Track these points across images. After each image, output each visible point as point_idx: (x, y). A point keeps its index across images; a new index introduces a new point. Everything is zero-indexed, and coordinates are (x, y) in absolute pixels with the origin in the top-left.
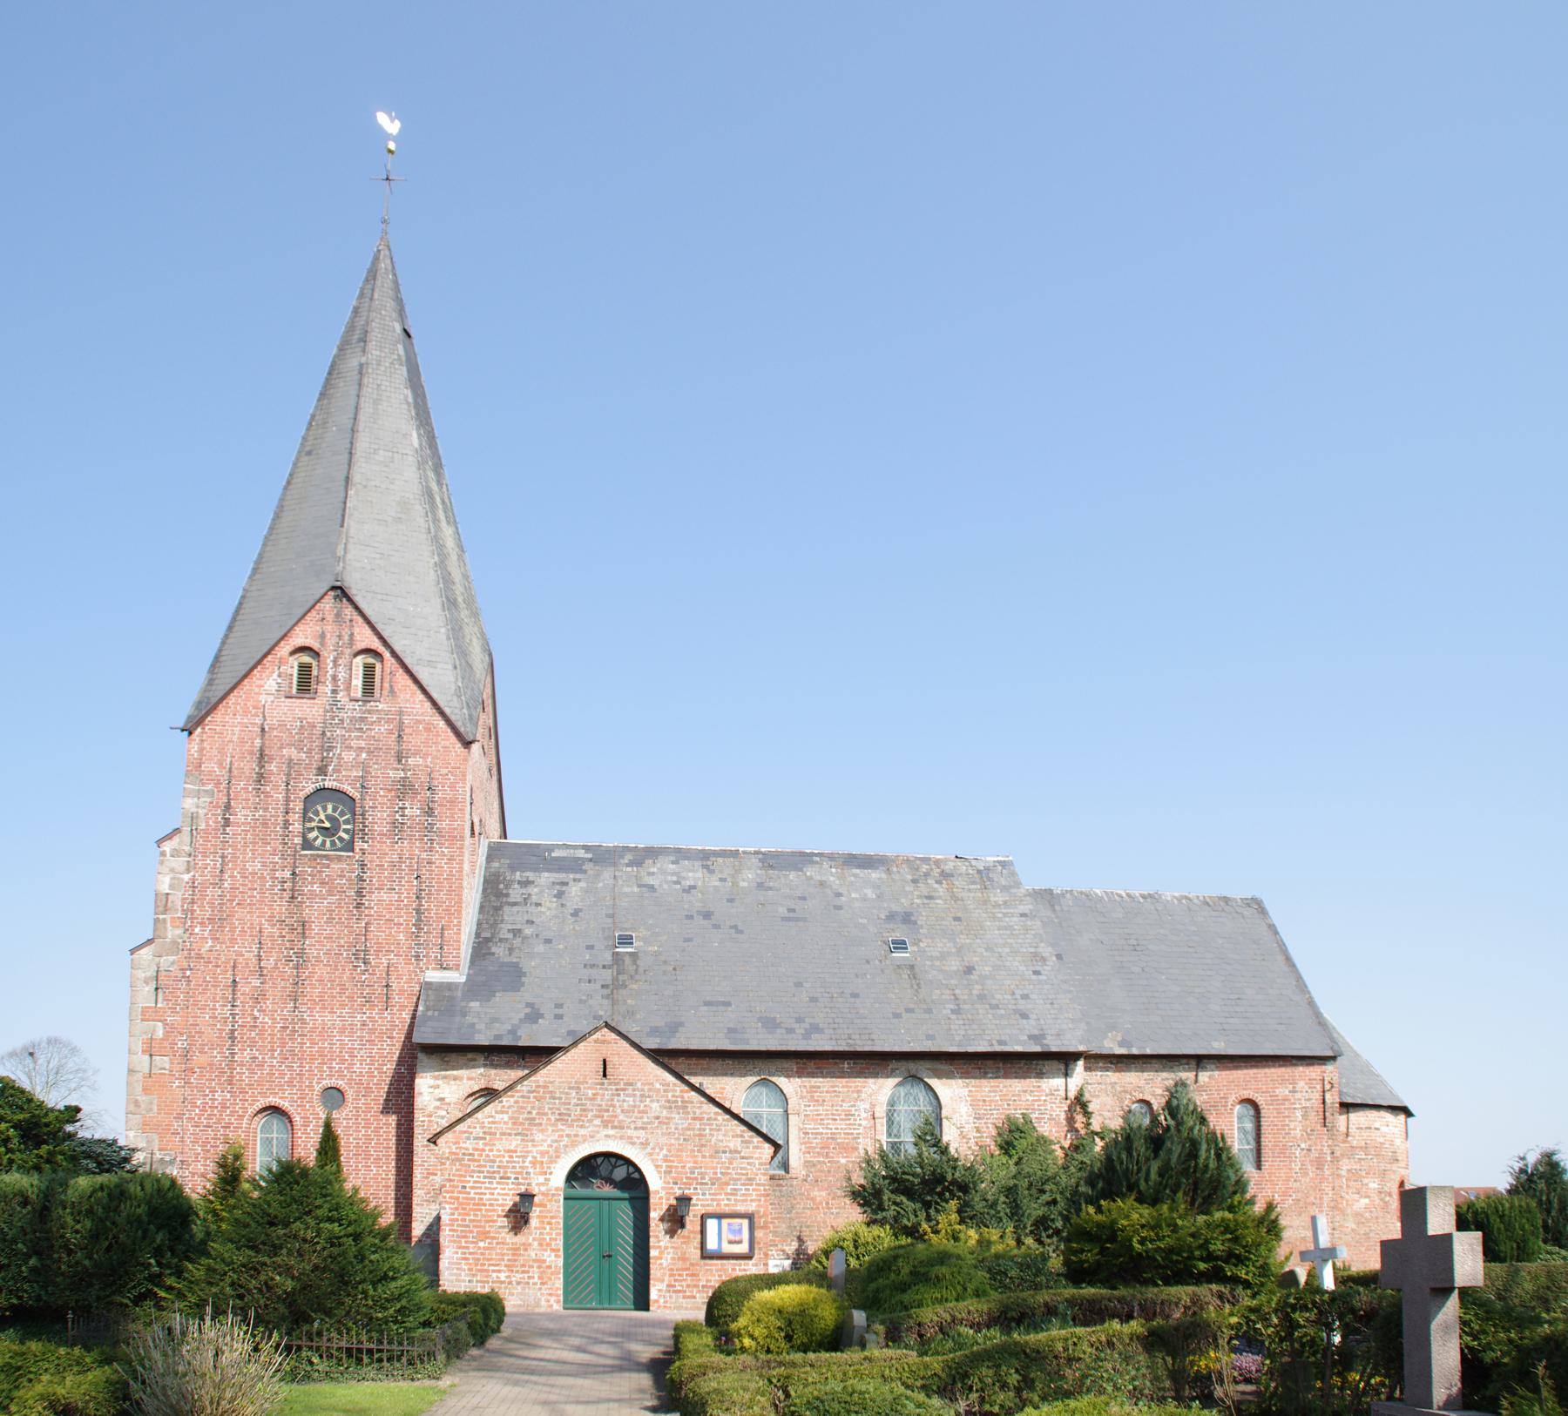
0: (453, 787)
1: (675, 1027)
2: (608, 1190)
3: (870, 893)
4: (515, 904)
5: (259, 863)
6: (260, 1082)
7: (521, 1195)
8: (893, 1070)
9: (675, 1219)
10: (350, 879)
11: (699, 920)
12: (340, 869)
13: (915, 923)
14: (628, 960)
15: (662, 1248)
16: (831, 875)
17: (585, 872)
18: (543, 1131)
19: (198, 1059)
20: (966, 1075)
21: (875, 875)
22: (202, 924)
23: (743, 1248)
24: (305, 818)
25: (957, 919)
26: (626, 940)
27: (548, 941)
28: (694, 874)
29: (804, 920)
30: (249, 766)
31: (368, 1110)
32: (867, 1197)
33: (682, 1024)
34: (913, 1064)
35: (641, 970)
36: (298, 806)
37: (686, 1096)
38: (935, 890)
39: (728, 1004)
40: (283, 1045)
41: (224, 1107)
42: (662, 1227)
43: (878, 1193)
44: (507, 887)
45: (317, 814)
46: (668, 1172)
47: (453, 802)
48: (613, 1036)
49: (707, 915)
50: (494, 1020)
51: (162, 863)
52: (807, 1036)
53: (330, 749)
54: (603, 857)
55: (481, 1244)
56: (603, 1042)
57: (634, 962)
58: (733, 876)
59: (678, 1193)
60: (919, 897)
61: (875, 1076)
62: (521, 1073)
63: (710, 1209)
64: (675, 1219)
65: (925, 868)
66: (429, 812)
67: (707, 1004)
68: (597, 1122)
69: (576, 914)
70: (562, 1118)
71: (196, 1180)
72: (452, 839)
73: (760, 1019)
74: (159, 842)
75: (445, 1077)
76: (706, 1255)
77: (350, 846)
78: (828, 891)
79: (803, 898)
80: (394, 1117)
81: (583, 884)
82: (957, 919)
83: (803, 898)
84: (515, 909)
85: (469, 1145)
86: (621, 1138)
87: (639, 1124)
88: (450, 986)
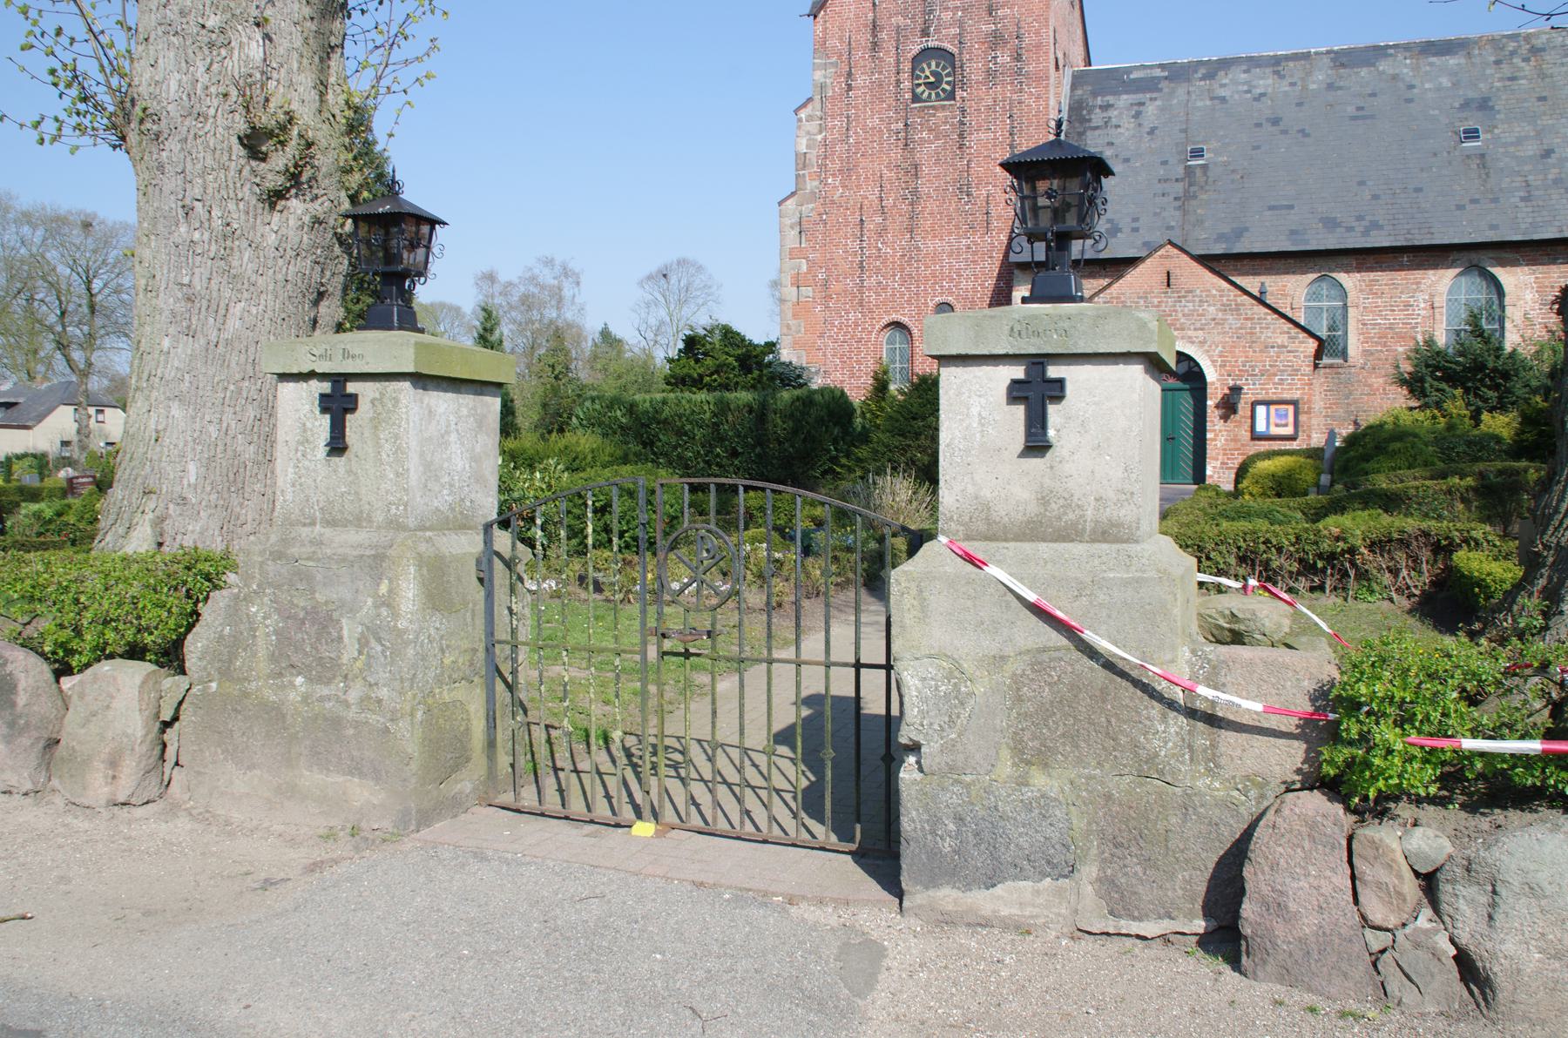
0: (1037, 33)
1: (1239, 233)
3: (1445, 82)
4: (1097, 128)
5: (877, 119)
6: (884, 303)
7: (1230, 389)
8: (1454, 261)
9: (1228, 407)
10: (952, 124)
11: (1268, 128)
12: (944, 117)
13: (1492, 108)
14: (1198, 172)
15: (1218, 432)
16: (1404, 67)
17: (1160, 90)
19: (835, 287)
20: (1533, 262)
21: (1452, 61)
22: (834, 175)
23: (1289, 430)
24: (914, 76)
25: (1542, 99)
26: (1198, 153)
27: (1127, 160)
28: (1265, 82)
29: (1372, 117)
30: (864, 38)
32: (1413, 385)
33: (1246, 229)
34: (1476, 256)
36: (907, 66)
38: (1520, 69)
39: (1291, 207)
40: (902, 270)
41: (857, 325)
43: (1422, 380)
44: (1089, 113)
45: (923, 71)
47: (1039, 46)
48: (1176, 251)
49: (1275, 122)
51: (799, 128)
52: (1366, 233)
53: (931, 12)
54: (1178, 73)
56: (1167, 257)
57: (1205, 173)
58: (1303, 79)
59: (1231, 383)
60: (1501, 79)
61: (1435, 267)
62: (1105, 282)
63: (1260, 397)
64: (1228, 407)
65: (1512, 45)
66: (1018, 58)
67: (1271, 208)
69: (1152, 132)
71: (857, 391)
72: (1039, 79)
73: (1321, 220)
74: (796, 112)
76: (1256, 437)
77: (951, 96)
78: (1401, 85)
79: (1373, 95)
81: (1158, 103)
82: (1542, 99)
83: (1373, 95)
84: (1097, 132)
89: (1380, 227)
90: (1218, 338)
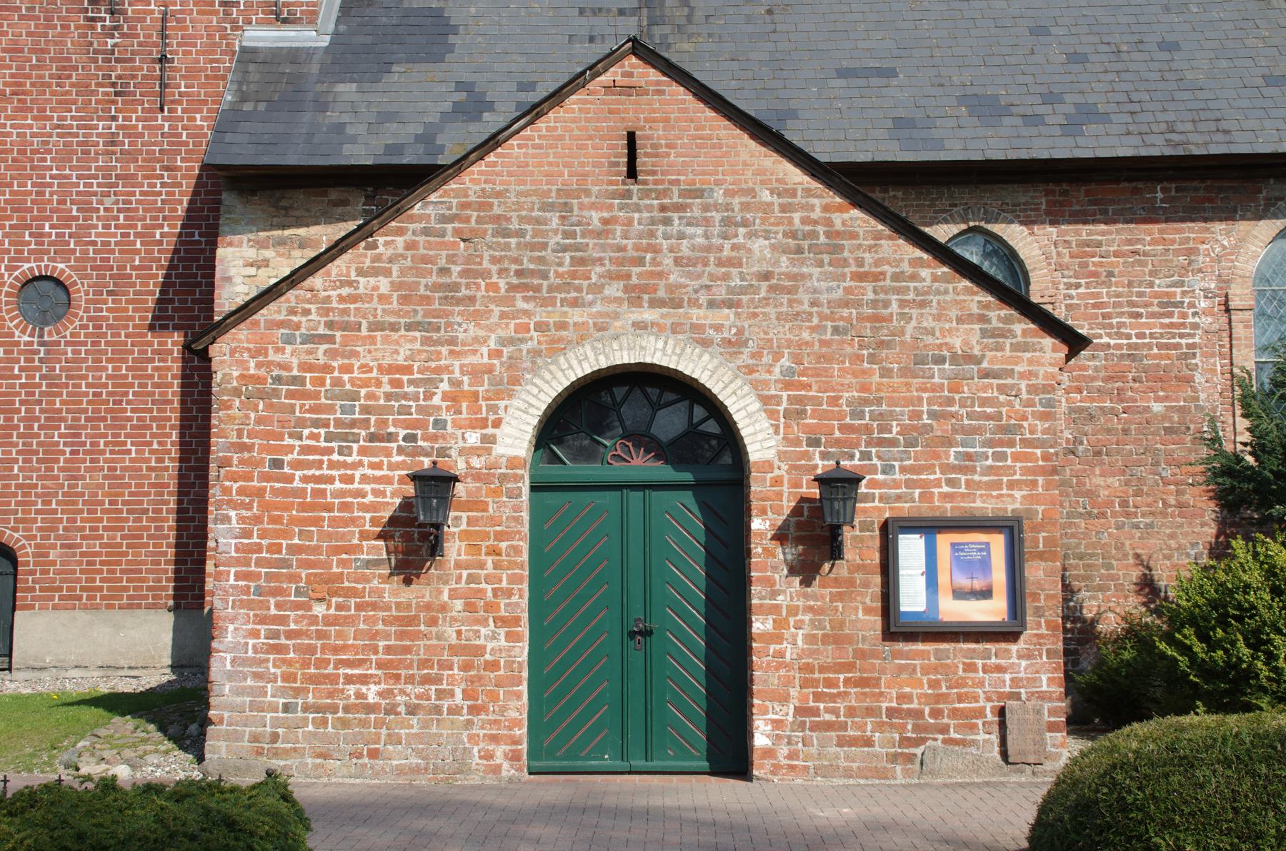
2: (642, 466)
7: (822, 481)
18: (476, 317)
23: (993, 610)
31: (121, 318)
35: (699, 15)
37: (837, 219)
39: (891, 73)
42: (781, 555)
46: (795, 414)
48: (653, 75)
50: (386, 117)
52: (1071, 127)
55: (319, 610)
56: (629, 89)
59: (822, 466)
61: (1229, 215)
67: (843, 73)
68: (615, 290)
70: (526, 282)
73: (962, 100)
75: (281, 242)
76: (897, 628)
80: (177, 337)
85: (291, 356)
86: (675, 329)
87: (721, 293)
88: (294, 56)
89: (1104, 118)
90: (781, 332)
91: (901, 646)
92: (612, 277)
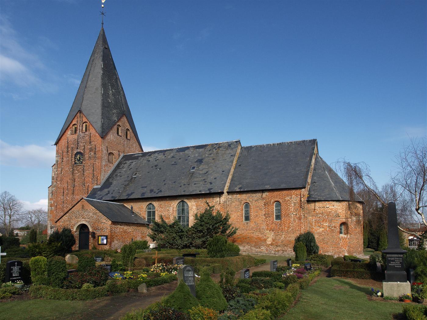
18: (73, 220)
46: (93, 227)
68: (81, 218)
86: (85, 221)
91: (99, 246)
92: (81, 217)
